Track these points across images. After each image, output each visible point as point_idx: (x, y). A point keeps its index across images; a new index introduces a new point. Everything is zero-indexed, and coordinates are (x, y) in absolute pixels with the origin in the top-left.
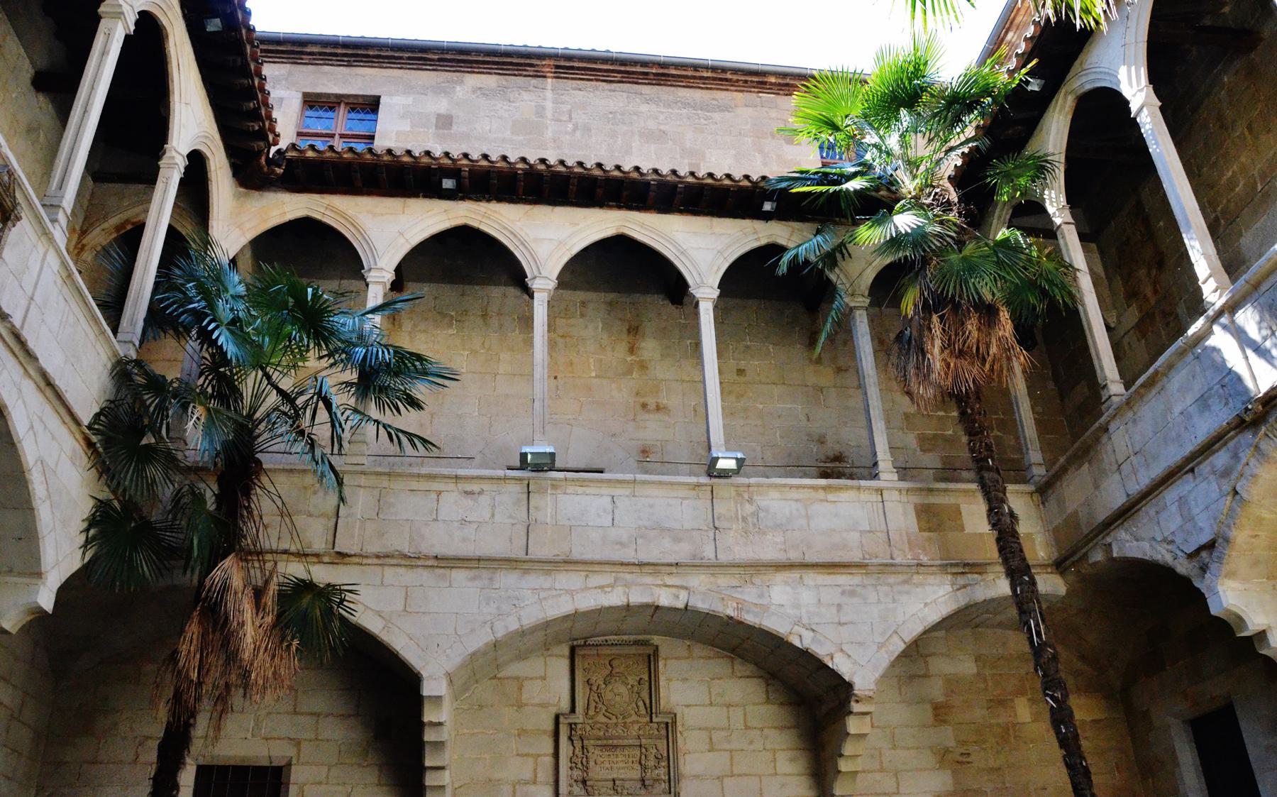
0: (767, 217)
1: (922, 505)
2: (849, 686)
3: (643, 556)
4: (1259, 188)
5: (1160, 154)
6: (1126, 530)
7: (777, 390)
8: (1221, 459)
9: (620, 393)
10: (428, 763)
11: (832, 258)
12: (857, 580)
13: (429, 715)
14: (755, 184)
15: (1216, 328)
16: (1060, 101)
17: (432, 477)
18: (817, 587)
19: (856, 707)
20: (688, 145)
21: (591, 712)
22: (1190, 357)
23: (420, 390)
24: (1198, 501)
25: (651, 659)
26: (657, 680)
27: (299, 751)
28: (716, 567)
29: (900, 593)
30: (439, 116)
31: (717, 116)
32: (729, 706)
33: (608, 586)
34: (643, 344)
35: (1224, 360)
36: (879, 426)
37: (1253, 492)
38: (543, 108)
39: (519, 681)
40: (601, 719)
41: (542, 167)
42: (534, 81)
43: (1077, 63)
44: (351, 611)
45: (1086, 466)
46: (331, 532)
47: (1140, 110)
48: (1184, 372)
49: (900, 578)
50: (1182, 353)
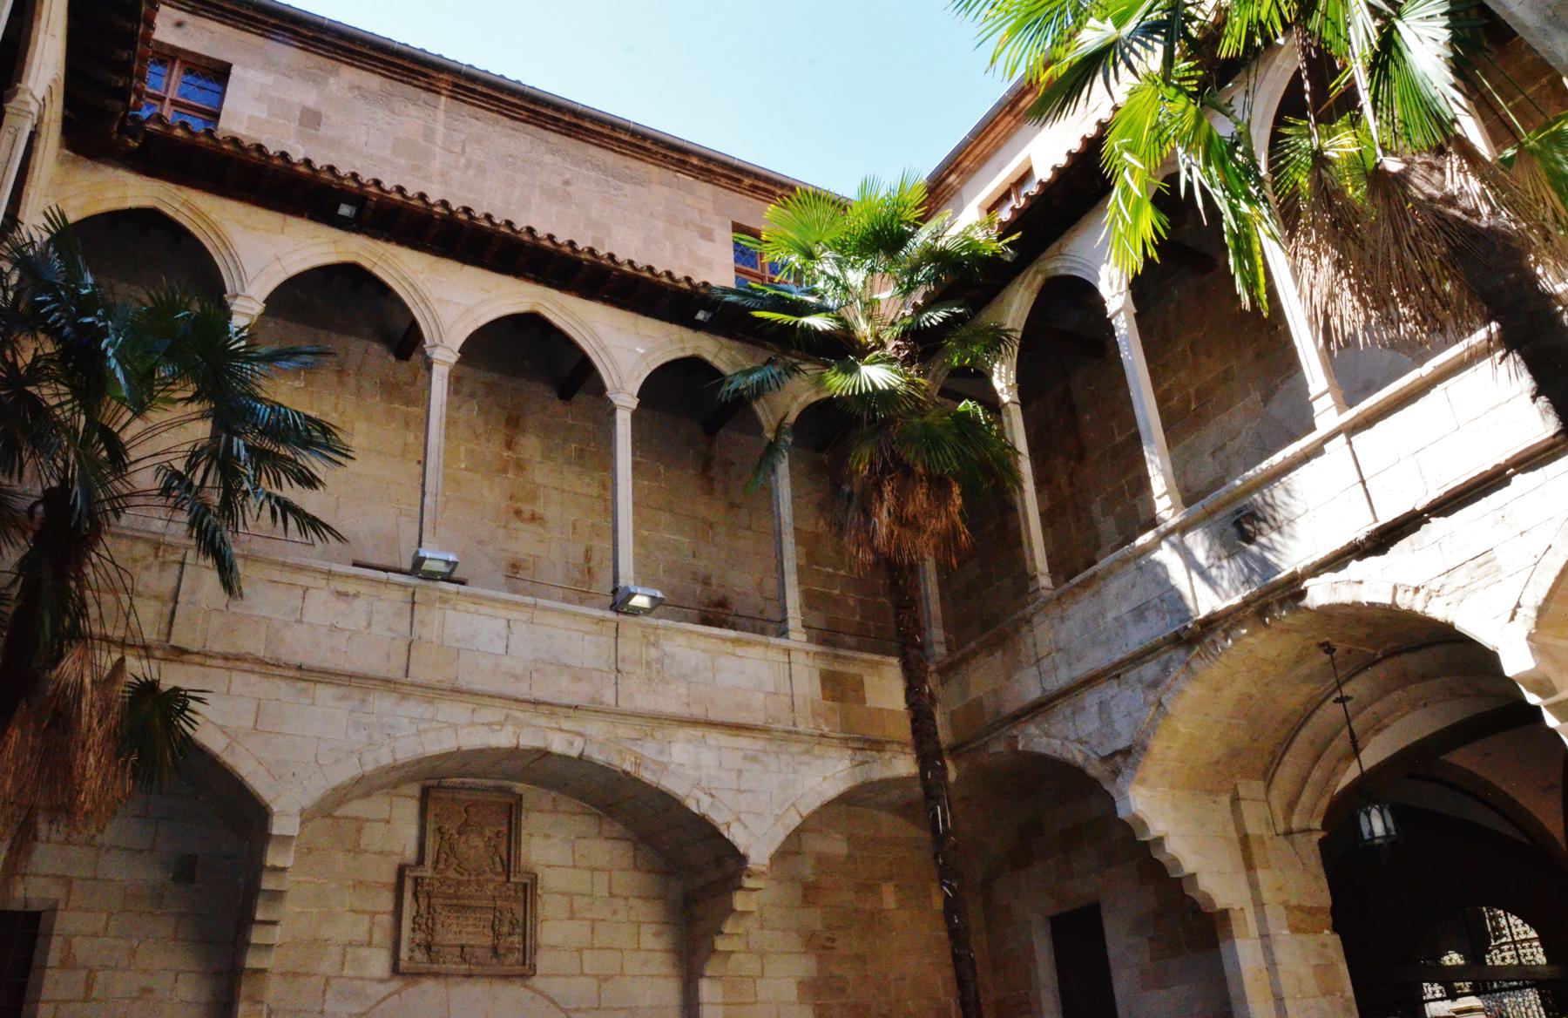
0: (696, 326)
1: (828, 672)
2: (743, 859)
3: (538, 694)
4: (1193, 407)
5: (1131, 363)
6: (1037, 726)
7: (665, 517)
8: (1150, 670)
9: (491, 493)
10: (259, 916)
11: (759, 390)
12: (759, 744)
13: (273, 858)
14: (695, 287)
15: (1164, 545)
16: (1030, 276)
17: (300, 569)
18: (719, 748)
19: (748, 883)
20: (594, 214)
21: (442, 866)
22: (1132, 566)
23: (315, 464)
24: (1124, 705)
25: (512, 811)
26: (518, 834)
27: (69, 892)
28: (617, 714)
29: (800, 763)
30: (305, 110)
31: (629, 188)
32: (593, 869)
33: (498, 723)
34: (523, 440)
35: (1168, 576)
36: (791, 579)
37: (1173, 705)
38: (432, 131)
39: (360, 823)
40: (451, 874)
41: (464, 217)
42: (424, 95)
43: (1055, 246)
44: (192, 723)
45: (999, 654)
46: (167, 619)
47: (1117, 313)
48: (1124, 580)
49: (804, 747)
50: (1125, 561)
